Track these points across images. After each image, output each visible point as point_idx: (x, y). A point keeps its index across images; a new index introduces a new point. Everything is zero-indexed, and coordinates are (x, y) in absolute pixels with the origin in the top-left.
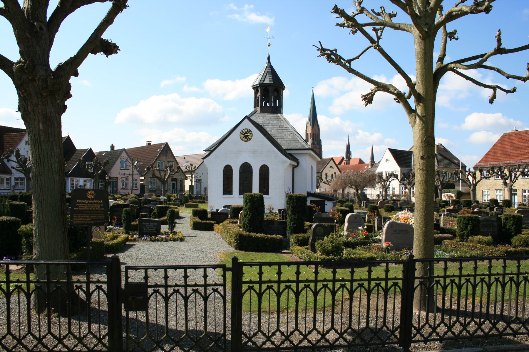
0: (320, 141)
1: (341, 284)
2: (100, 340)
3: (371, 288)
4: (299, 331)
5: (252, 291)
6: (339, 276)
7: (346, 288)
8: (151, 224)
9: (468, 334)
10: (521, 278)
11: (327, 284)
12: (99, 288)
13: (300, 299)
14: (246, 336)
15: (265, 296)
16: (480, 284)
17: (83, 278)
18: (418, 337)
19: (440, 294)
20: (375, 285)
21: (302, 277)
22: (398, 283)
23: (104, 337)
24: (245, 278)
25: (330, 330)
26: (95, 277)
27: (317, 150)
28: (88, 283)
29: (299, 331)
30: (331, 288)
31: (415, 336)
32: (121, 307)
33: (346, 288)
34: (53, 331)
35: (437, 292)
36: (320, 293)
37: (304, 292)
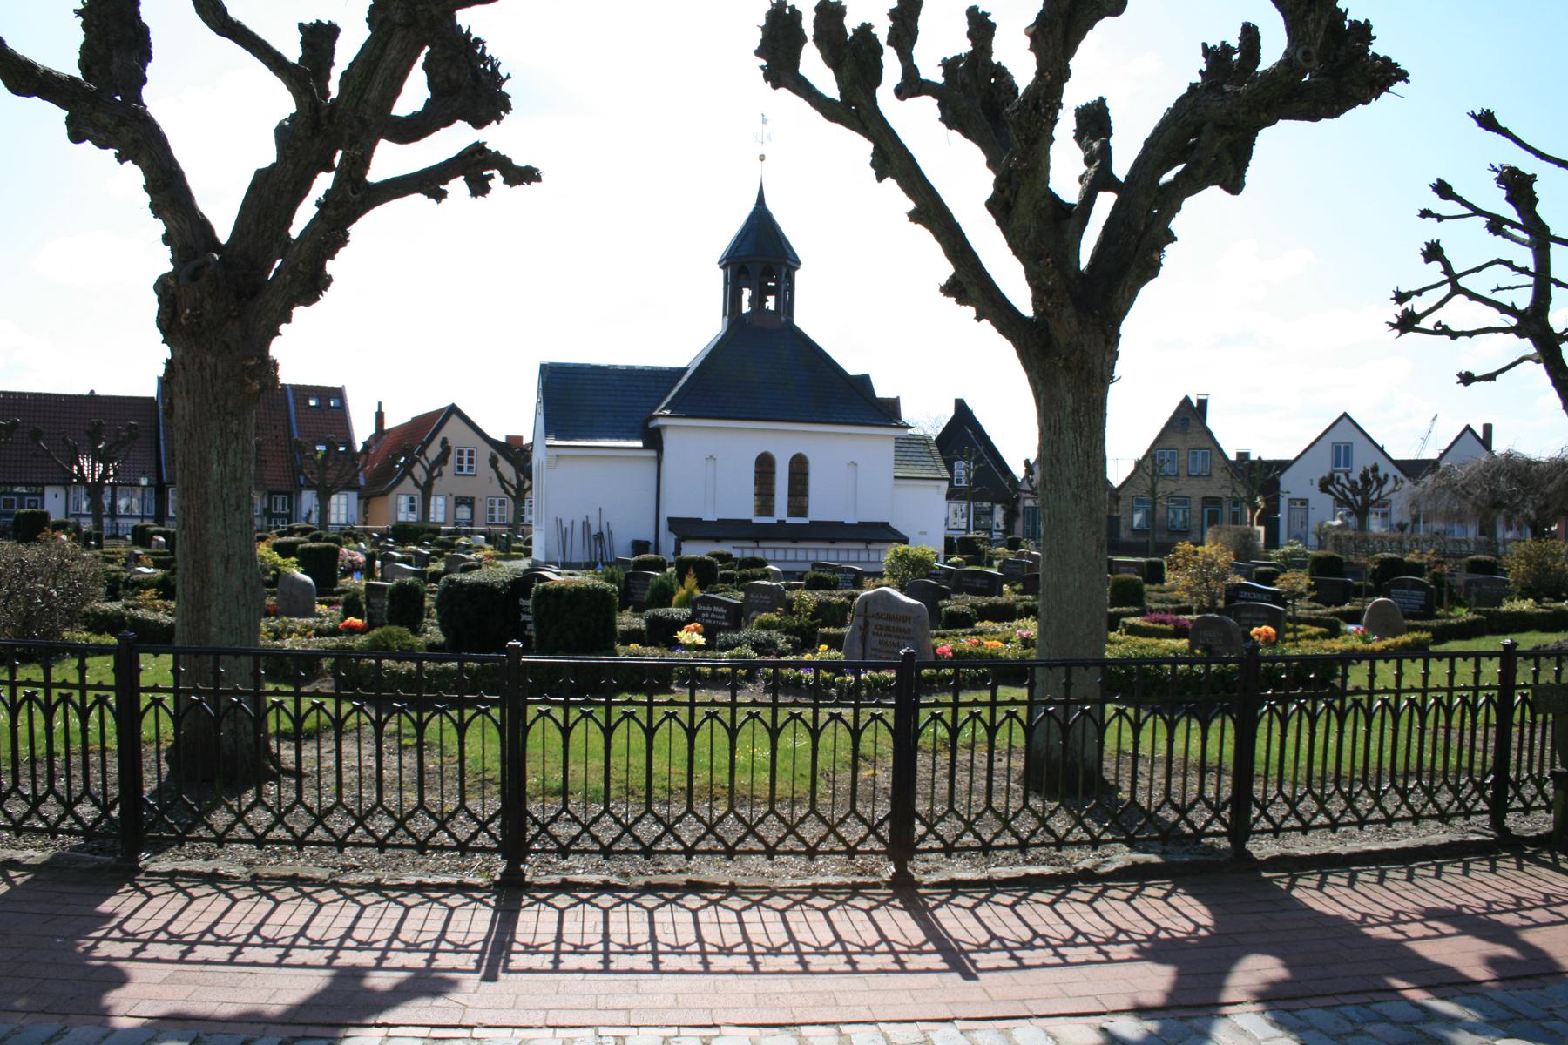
0: (862, 525)
1: (831, 714)
2: (873, 830)
3: (738, 724)
4: (695, 815)
5: (633, 723)
6: (57, 676)
7: (678, 721)
8: (716, 609)
9: (529, 837)
10: (1000, 715)
11: (322, 703)
12: (101, 701)
13: (697, 740)
14: (923, 822)
15: (743, 738)
16: (1115, 723)
17: (723, 696)
18: (1264, 824)
19: (981, 742)
20: (310, 706)
21: (91, 679)
22: (161, 699)
23: (881, 822)
24: (145, 680)
25: (1196, 801)
26: (1004, 693)
27: (894, 537)
28: (734, 705)
29: (695, 815)
30: (78, 703)
31: (1257, 820)
32: (1494, 757)
33: (678, 721)
34: (860, 808)
35: (129, 719)
36: (577, 728)
37: (748, 727)
